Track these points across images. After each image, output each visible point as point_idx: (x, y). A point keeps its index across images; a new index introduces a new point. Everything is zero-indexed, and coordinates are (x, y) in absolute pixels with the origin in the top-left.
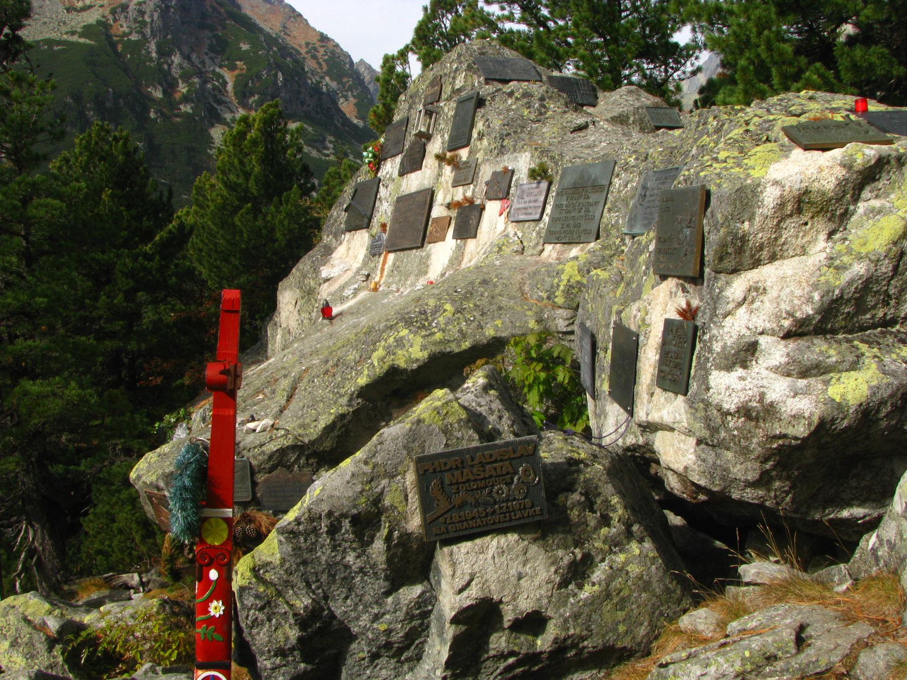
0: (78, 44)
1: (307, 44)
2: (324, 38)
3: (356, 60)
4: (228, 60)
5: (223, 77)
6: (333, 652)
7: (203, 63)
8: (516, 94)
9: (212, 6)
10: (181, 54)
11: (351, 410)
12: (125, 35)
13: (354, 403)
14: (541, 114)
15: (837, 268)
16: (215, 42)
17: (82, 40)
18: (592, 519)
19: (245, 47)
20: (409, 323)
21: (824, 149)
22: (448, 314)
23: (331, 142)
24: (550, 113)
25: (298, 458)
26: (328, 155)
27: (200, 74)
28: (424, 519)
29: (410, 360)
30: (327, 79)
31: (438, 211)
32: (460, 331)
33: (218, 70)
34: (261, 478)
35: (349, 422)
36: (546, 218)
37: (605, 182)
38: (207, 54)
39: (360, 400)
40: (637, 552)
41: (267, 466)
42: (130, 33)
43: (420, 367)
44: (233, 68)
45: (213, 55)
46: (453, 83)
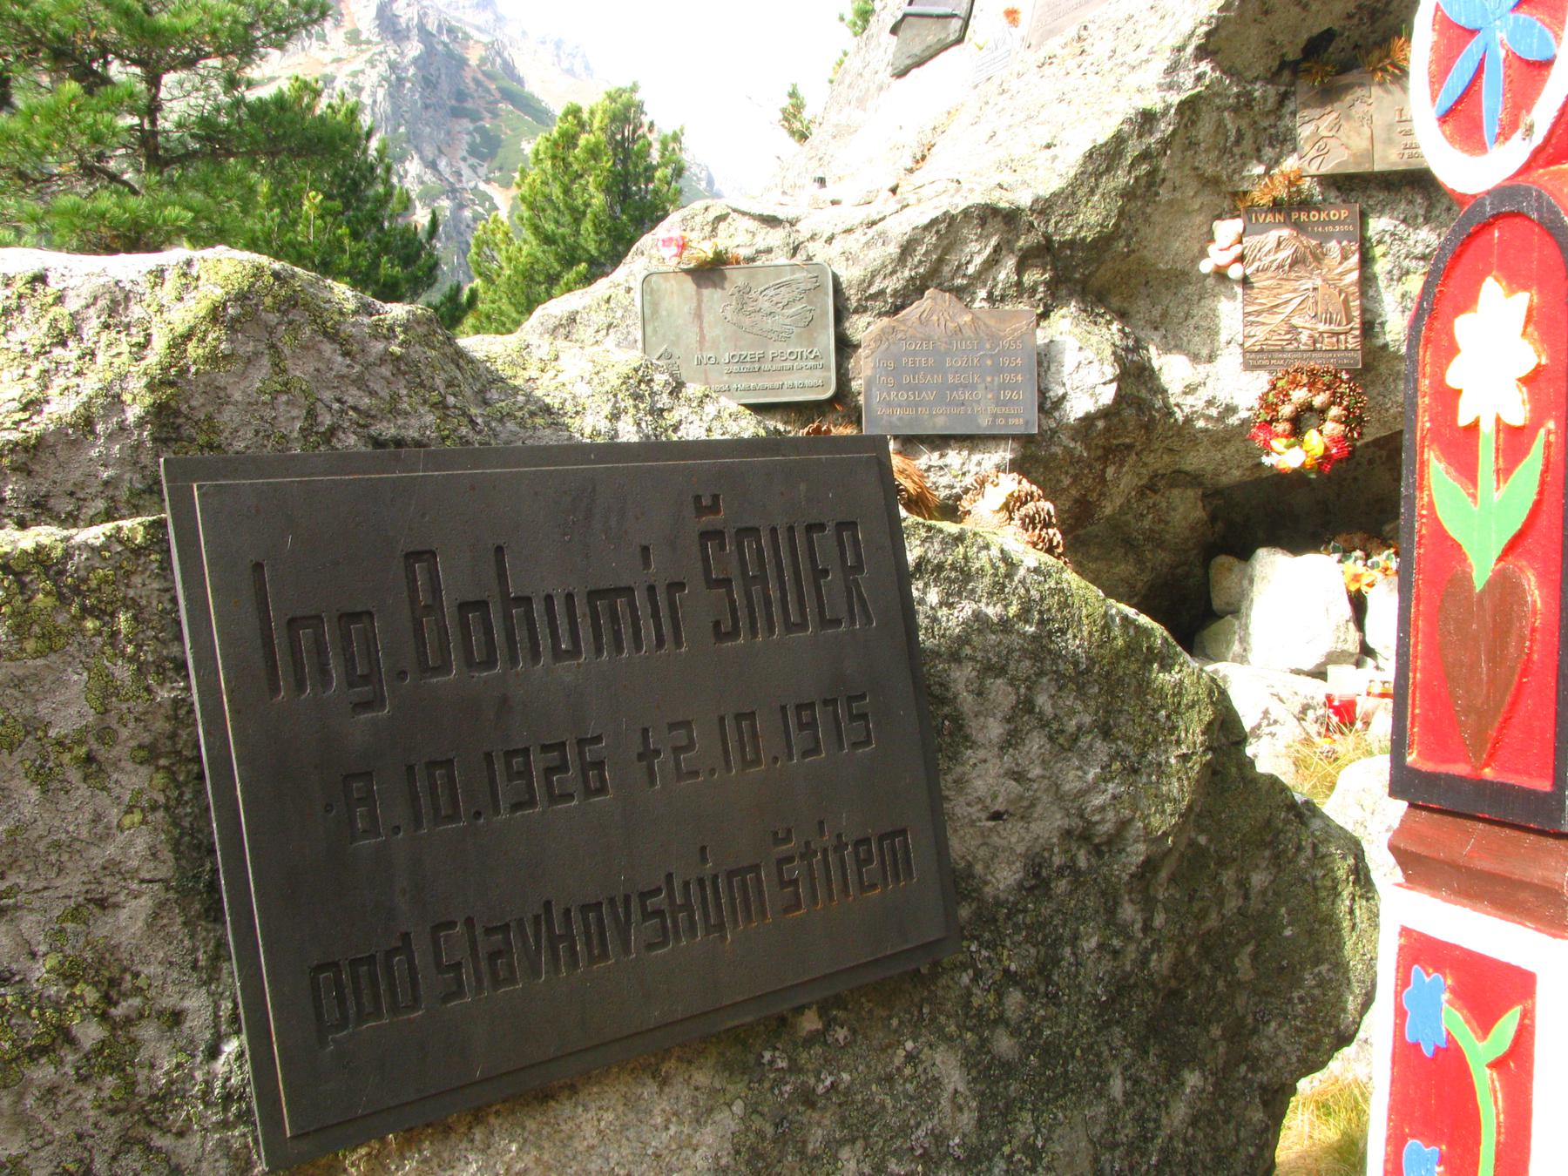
4: (500, 169)
5: (490, 199)
6: (1533, 579)
7: (459, 174)
9: (476, 80)
10: (421, 158)
11: (1175, 98)
13: (1186, 78)
16: (478, 140)
25: (993, 262)
27: (453, 192)
33: (482, 186)
34: (862, 328)
35: (1166, 143)
38: (464, 159)
39: (1205, 66)
41: (892, 284)
44: (506, 184)
45: (474, 161)
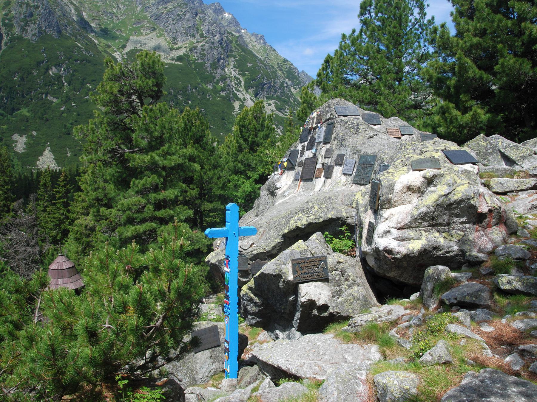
0: (175, 64)
1: (278, 64)
2: (285, 61)
3: (300, 70)
5: (239, 79)
8: (348, 123)
12: (196, 60)
14: (357, 131)
15: (417, 209)
17: (177, 63)
18: (343, 279)
19: (249, 65)
20: (303, 211)
21: (420, 171)
22: (316, 209)
23: (288, 109)
24: (360, 131)
26: (286, 115)
28: (294, 276)
29: (302, 225)
30: (287, 80)
31: (319, 166)
32: (319, 215)
36: (354, 174)
37: (373, 163)
40: (356, 289)
42: (198, 59)
43: (305, 227)
45: (235, 69)
46: (326, 116)
